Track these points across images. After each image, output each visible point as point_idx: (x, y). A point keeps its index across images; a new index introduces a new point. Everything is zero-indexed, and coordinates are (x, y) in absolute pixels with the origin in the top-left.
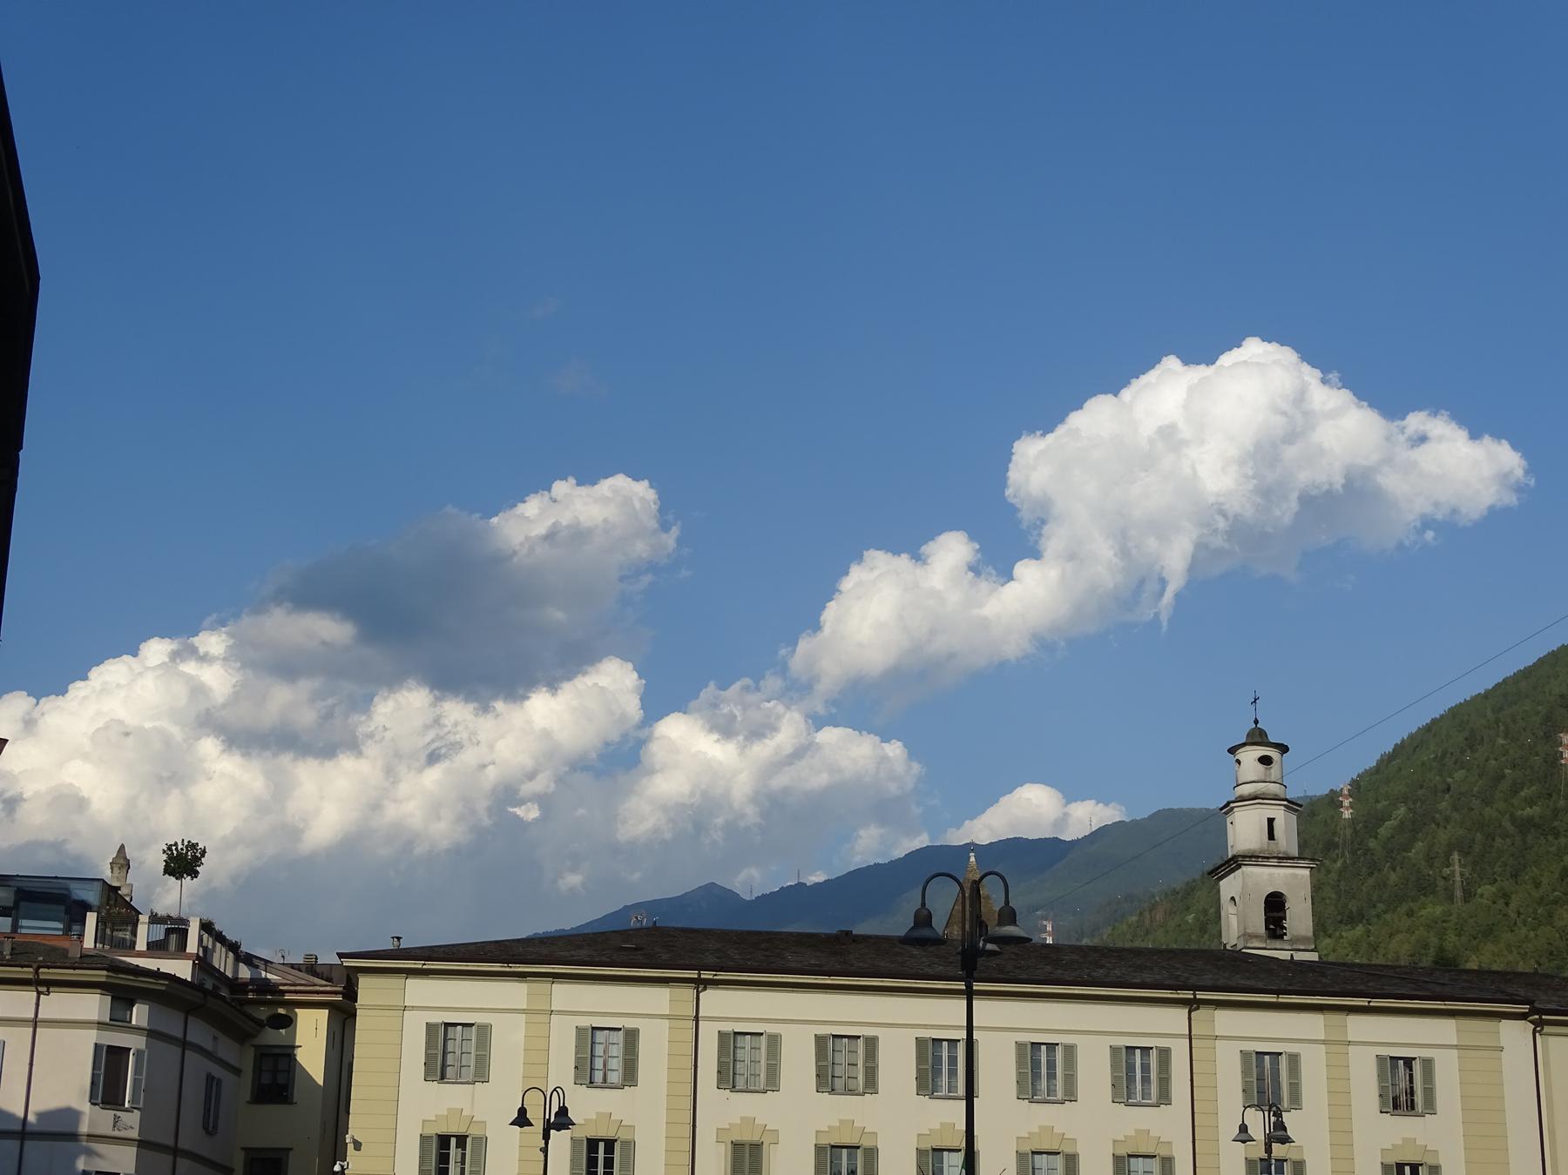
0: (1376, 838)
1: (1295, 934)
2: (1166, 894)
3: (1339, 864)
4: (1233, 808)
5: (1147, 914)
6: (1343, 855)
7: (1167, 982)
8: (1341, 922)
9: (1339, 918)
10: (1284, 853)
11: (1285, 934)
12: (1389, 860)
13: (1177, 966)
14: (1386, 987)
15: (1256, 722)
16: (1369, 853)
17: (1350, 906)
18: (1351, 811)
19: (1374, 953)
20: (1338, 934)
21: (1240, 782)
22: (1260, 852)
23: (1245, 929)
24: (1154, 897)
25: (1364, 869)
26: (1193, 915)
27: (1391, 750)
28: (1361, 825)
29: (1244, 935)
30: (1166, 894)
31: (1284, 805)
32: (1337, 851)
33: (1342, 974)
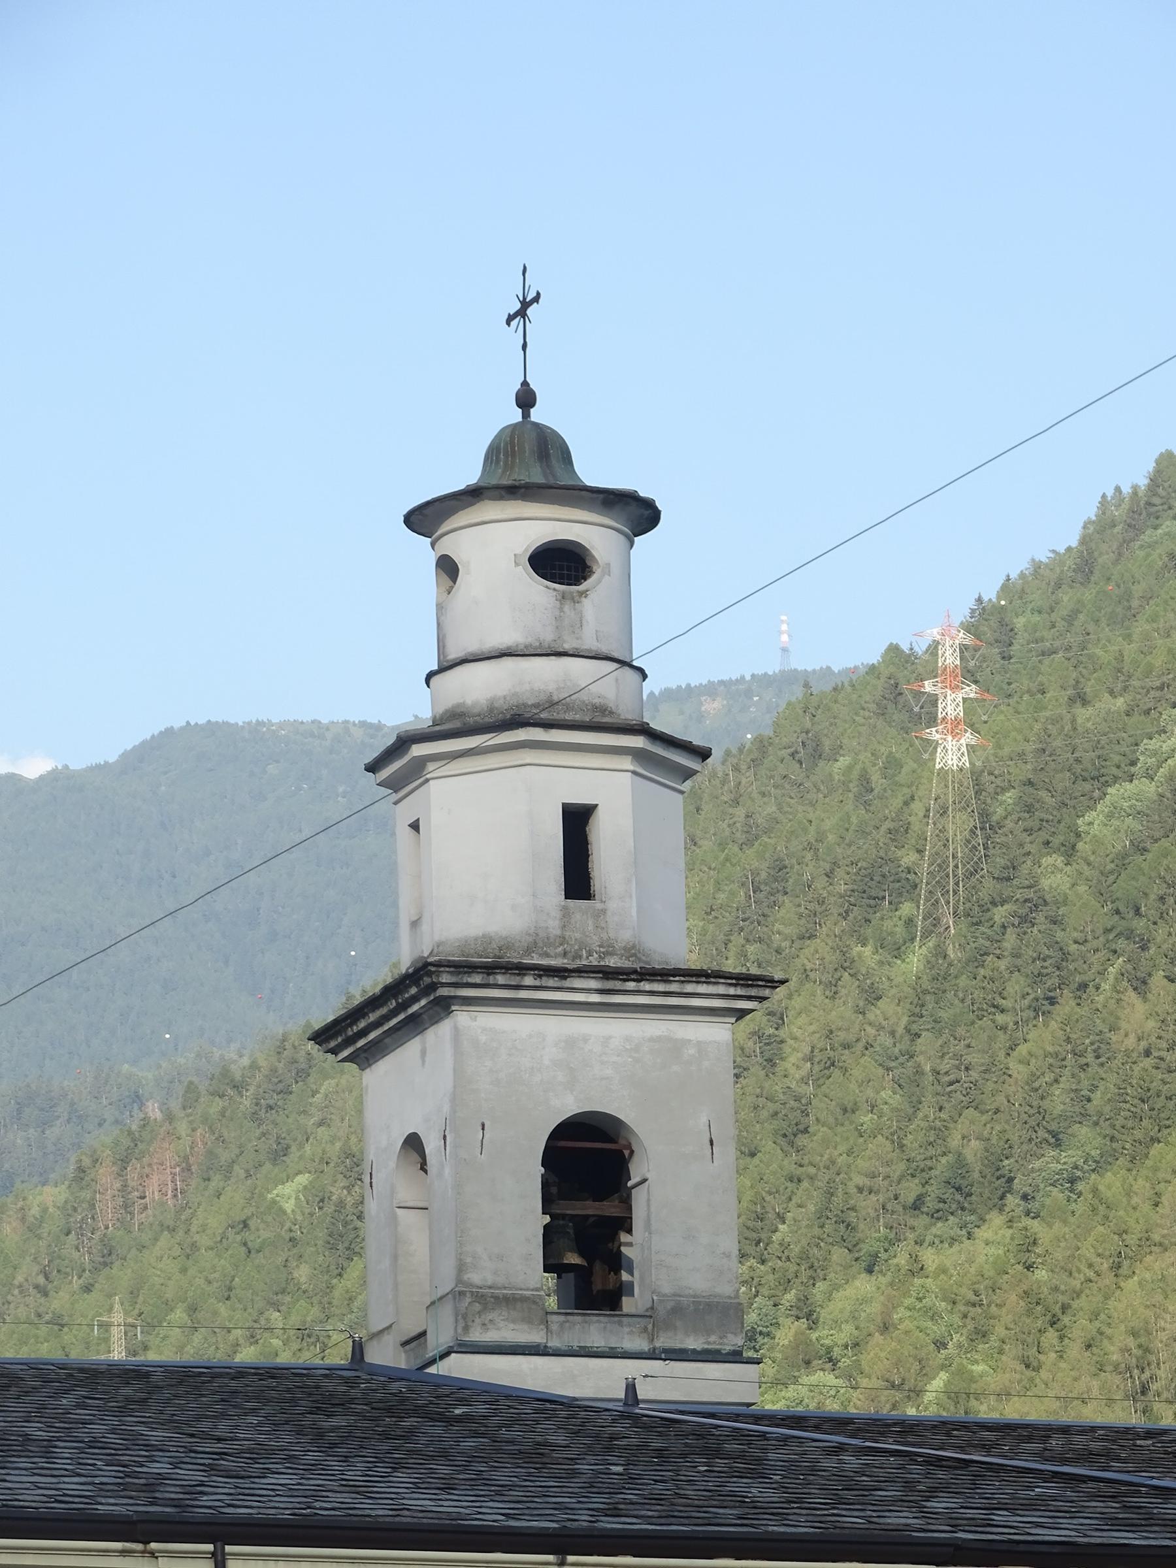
0: (1069, 851)
1: (667, 1289)
2: (191, 1088)
3: (915, 960)
4: (420, 764)
5: (105, 1175)
6: (934, 922)
7: (108, 1506)
8: (917, 1205)
9: (910, 1190)
10: (631, 951)
11: (628, 1289)
12: (1121, 944)
13: (157, 1435)
14: (1000, 1517)
15: (526, 399)
16: (1040, 918)
17: (955, 1141)
18: (968, 738)
19: (1051, 1335)
20: (902, 1260)
21: (453, 654)
22: (528, 951)
23: (461, 1268)
24: (138, 1099)
25: (1016, 985)
26: (303, 1179)
27: (1143, 482)
28: (1009, 797)
29: (457, 1295)
30: (191, 1088)
31: (638, 755)
32: (907, 909)
33: (829, 1463)
